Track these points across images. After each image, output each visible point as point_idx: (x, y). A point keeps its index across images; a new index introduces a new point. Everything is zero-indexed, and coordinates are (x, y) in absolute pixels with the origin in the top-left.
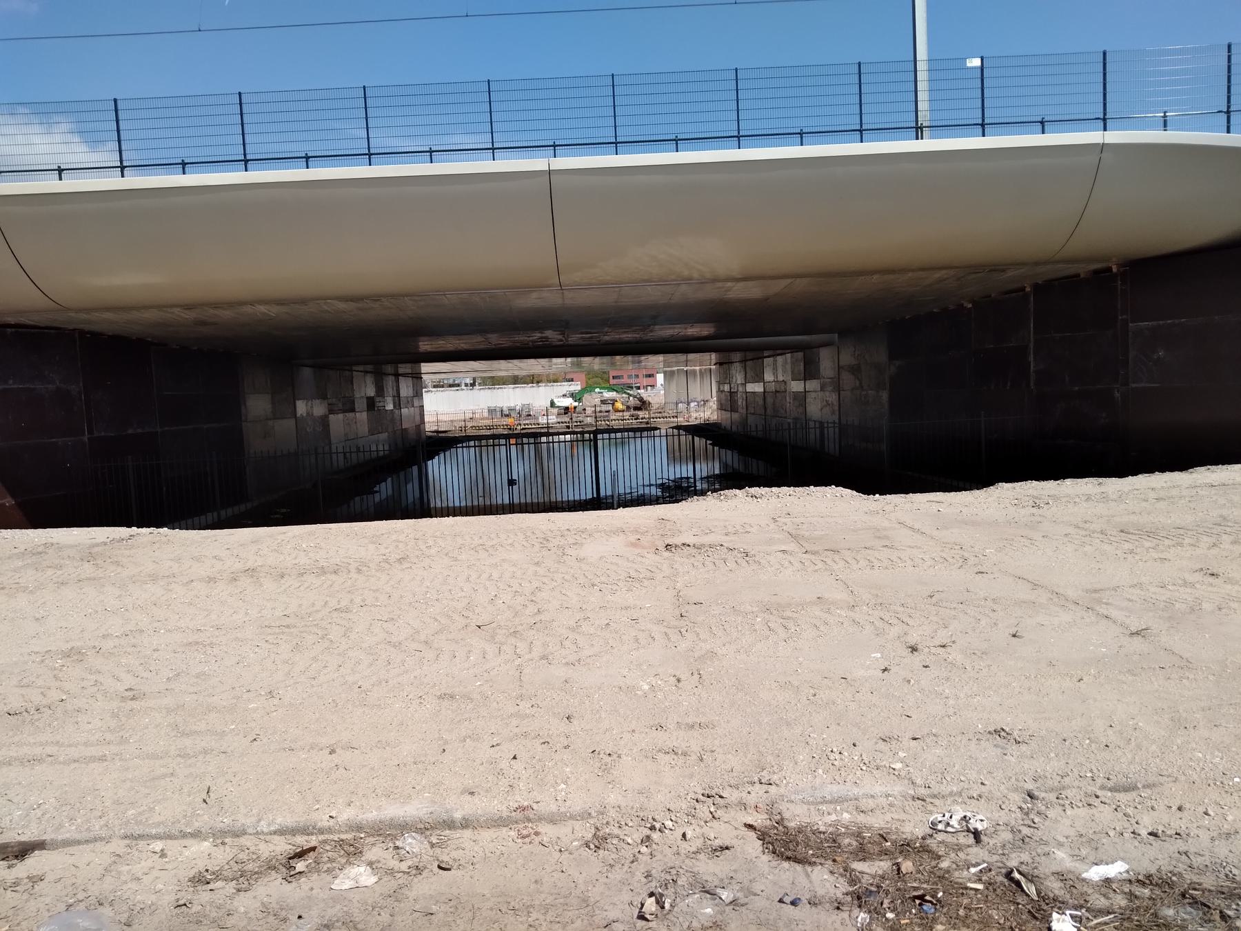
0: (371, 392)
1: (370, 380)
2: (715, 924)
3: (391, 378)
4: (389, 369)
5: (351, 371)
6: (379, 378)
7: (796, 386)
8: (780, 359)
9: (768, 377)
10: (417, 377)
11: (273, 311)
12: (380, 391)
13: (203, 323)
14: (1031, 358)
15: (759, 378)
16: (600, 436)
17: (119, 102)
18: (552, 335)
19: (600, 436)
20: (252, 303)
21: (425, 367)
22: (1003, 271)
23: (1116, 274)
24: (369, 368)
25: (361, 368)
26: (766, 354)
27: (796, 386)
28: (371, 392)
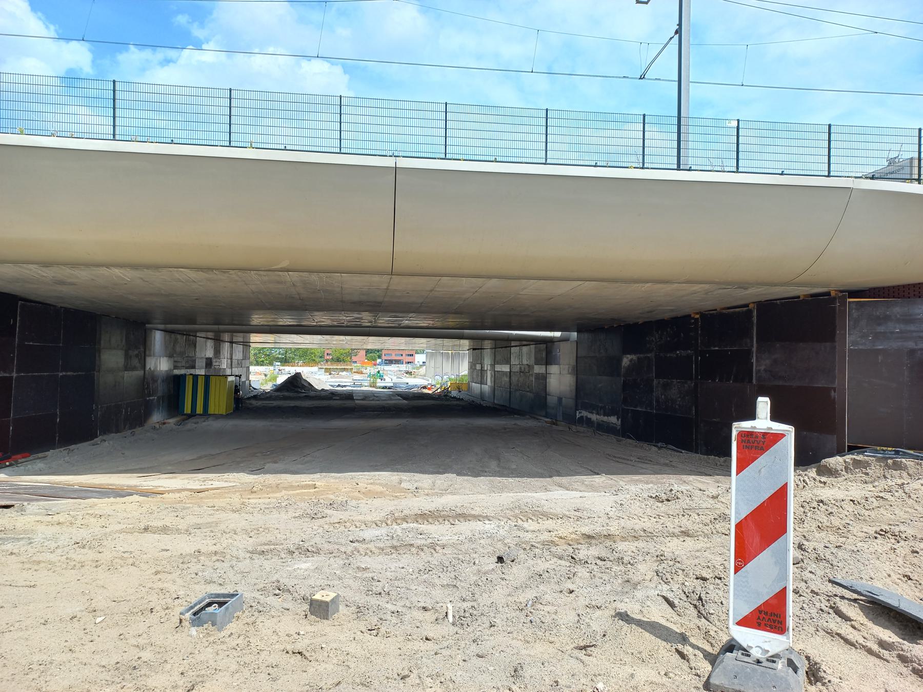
0: (210, 353)
1: (210, 344)
2: (311, 605)
3: (227, 345)
4: (226, 337)
5: (196, 336)
6: (218, 341)
7: (539, 369)
8: (525, 349)
9: (514, 361)
10: (246, 344)
11: (127, 275)
12: (217, 352)
13: (62, 283)
14: (754, 360)
15: (507, 361)
16: (916, 177)
17: (117, 84)
18: (366, 318)
19: (916, 177)
20: (108, 266)
21: (254, 338)
22: (746, 289)
23: (835, 298)
24: (210, 335)
25: (203, 334)
26: (513, 344)
27: (539, 369)
28: (210, 353)
